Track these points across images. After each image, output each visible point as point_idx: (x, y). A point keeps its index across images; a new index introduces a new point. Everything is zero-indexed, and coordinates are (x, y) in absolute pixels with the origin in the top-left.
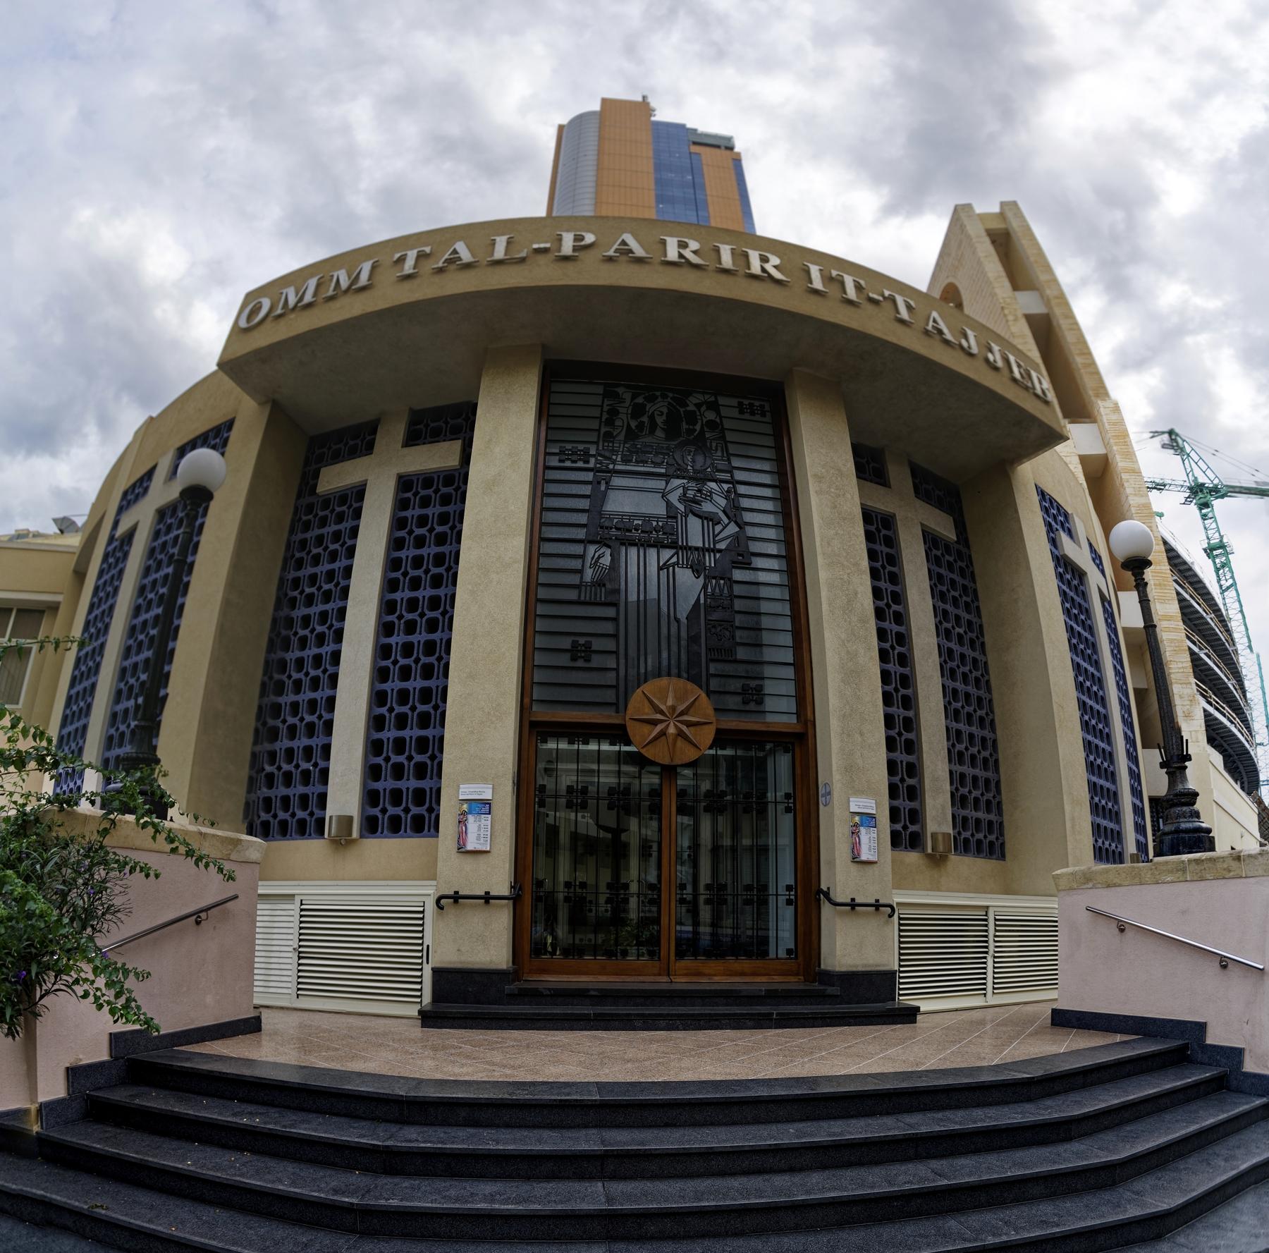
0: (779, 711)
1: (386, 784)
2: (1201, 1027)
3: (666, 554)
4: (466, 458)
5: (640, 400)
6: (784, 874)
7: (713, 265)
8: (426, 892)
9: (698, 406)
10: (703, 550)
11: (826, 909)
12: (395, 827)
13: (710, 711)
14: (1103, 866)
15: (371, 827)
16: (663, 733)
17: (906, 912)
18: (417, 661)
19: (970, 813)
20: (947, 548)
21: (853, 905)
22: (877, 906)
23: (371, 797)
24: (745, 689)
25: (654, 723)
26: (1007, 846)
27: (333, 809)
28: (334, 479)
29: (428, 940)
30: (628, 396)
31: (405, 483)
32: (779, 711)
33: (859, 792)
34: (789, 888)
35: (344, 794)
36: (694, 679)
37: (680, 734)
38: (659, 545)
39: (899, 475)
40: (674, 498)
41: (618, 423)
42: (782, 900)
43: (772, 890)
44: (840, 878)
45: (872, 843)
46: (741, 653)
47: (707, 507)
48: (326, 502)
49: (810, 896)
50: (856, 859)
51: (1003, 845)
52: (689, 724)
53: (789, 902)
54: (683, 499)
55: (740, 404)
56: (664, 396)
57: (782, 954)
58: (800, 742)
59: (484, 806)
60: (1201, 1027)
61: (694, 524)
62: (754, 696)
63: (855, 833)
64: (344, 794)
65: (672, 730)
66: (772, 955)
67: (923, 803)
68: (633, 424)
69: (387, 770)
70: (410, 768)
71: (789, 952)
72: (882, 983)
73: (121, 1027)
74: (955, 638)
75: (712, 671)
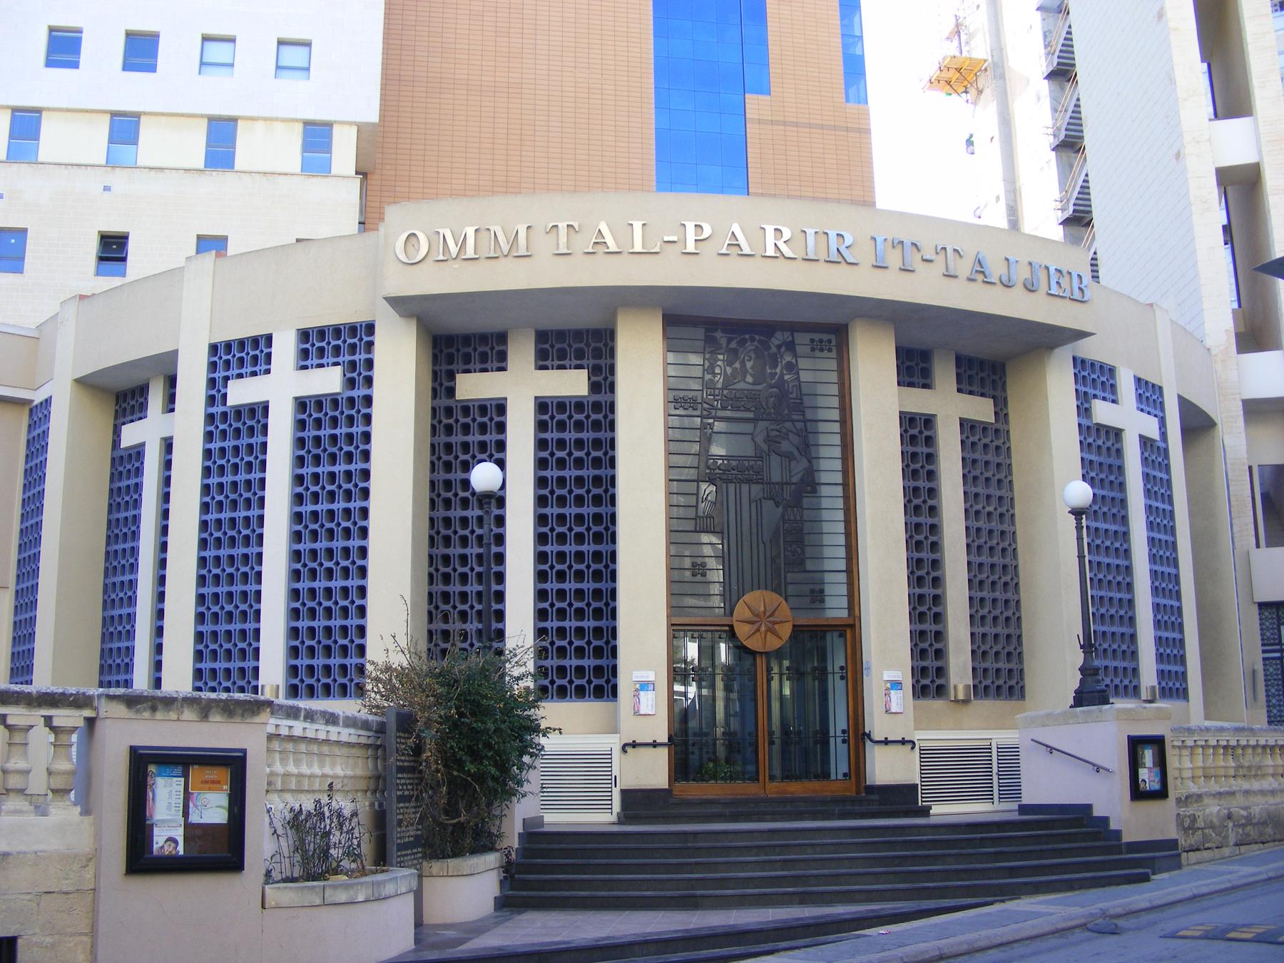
0: (836, 608)
3: (756, 489)
5: (733, 345)
6: (839, 721)
8: (612, 743)
9: (779, 347)
10: (782, 484)
11: (868, 743)
13: (788, 612)
17: (923, 744)
18: (345, 341)
20: (985, 428)
21: (886, 742)
22: (903, 742)
24: (812, 591)
26: (1027, 688)
28: (473, 386)
29: (616, 772)
31: (542, 405)
32: (836, 608)
33: (889, 668)
34: (844, 732)
36: (776, 590)
38: (749, 481)
39: (945, 375)
40: (759, 440)
41: (717, 371)
42: (839, 740)
43: (832, 733)
44: (877, 724)
45: (901, 700)
49: (859, 737)
51: (1022, 687)
52: (772, 615)
53: (844, 741)
54: (768, 440)
55: (812, 341)
57: (840, 777)
58: (850, 629)
59: (644, 686)
61: (775, 460)
62: (818, 596)
63: (637, 696)
65: (763, 628)
66: (833, 777)
67: (947, 662)
68: (729, 370)
71: (845, 775)
72: (908, 791)
74: (1099, 386)
75: (789, 580)
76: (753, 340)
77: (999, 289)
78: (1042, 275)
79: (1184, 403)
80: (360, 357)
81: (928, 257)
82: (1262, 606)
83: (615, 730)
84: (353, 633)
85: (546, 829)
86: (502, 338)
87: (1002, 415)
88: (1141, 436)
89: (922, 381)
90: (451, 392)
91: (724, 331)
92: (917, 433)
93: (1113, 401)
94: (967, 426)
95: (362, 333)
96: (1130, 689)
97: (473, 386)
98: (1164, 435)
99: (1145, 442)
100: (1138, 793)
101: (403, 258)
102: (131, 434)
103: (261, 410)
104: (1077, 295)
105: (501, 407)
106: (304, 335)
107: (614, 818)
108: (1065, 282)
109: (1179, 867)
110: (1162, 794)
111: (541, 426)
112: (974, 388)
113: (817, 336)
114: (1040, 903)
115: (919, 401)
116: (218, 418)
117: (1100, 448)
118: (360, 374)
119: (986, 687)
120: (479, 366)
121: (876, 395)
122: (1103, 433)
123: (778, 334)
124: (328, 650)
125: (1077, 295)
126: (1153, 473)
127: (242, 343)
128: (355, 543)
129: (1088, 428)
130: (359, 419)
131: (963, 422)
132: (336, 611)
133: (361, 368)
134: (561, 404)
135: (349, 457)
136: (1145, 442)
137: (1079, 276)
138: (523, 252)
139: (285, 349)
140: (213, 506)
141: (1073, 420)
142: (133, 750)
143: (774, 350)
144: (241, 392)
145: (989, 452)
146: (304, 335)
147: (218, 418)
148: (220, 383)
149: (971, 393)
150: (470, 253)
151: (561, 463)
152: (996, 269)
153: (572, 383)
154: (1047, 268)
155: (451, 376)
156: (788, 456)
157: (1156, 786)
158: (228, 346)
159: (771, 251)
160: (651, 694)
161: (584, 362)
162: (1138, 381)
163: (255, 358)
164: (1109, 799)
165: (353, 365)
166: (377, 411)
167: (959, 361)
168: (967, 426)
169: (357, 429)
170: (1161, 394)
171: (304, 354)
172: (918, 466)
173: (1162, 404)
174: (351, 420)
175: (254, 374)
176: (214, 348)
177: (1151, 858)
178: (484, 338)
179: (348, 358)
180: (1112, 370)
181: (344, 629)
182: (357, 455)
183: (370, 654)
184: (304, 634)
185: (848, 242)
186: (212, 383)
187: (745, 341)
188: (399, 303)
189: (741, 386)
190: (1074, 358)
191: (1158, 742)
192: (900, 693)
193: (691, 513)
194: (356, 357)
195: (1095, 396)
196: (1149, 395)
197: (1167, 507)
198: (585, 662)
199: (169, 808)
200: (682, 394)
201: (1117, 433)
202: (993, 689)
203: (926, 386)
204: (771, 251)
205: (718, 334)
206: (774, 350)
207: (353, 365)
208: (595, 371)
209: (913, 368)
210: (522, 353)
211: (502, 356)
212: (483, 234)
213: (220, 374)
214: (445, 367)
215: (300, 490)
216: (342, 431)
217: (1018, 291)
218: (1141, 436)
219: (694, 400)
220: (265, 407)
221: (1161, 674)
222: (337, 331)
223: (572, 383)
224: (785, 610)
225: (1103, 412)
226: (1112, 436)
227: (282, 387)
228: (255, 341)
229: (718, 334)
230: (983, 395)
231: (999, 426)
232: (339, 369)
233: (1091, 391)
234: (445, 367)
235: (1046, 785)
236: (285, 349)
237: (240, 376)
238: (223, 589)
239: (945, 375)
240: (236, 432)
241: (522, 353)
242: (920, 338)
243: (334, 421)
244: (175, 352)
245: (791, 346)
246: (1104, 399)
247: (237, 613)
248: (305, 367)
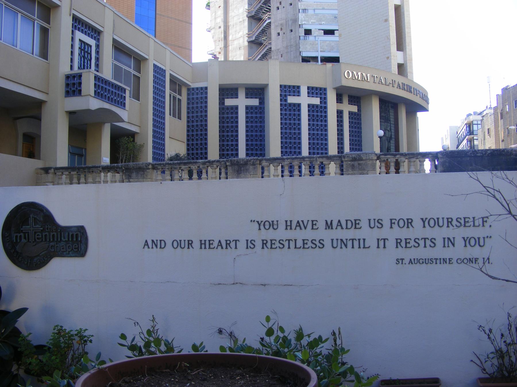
20: (355, 113)
28: (229, 102)
31: (247, 107)
39: (346, 100)
92: (340, 113)
94: (350, 113)
124: (197, 149)
135: (201, 149)
139: (304, 91)
145: (356, 120)
151: (252, 122)
153: (255, 102)
167: (349, 96)
168: (350, 113)
169: (203, 114)
174: (201, 149)
181: (201, 98)
182: (204, 149)
203: (298, 96)
208: (260, 99)
210: (242, 94)
214: (222, 97)
223: (255, 102)
239: (346, 100)
241: (242, 94)
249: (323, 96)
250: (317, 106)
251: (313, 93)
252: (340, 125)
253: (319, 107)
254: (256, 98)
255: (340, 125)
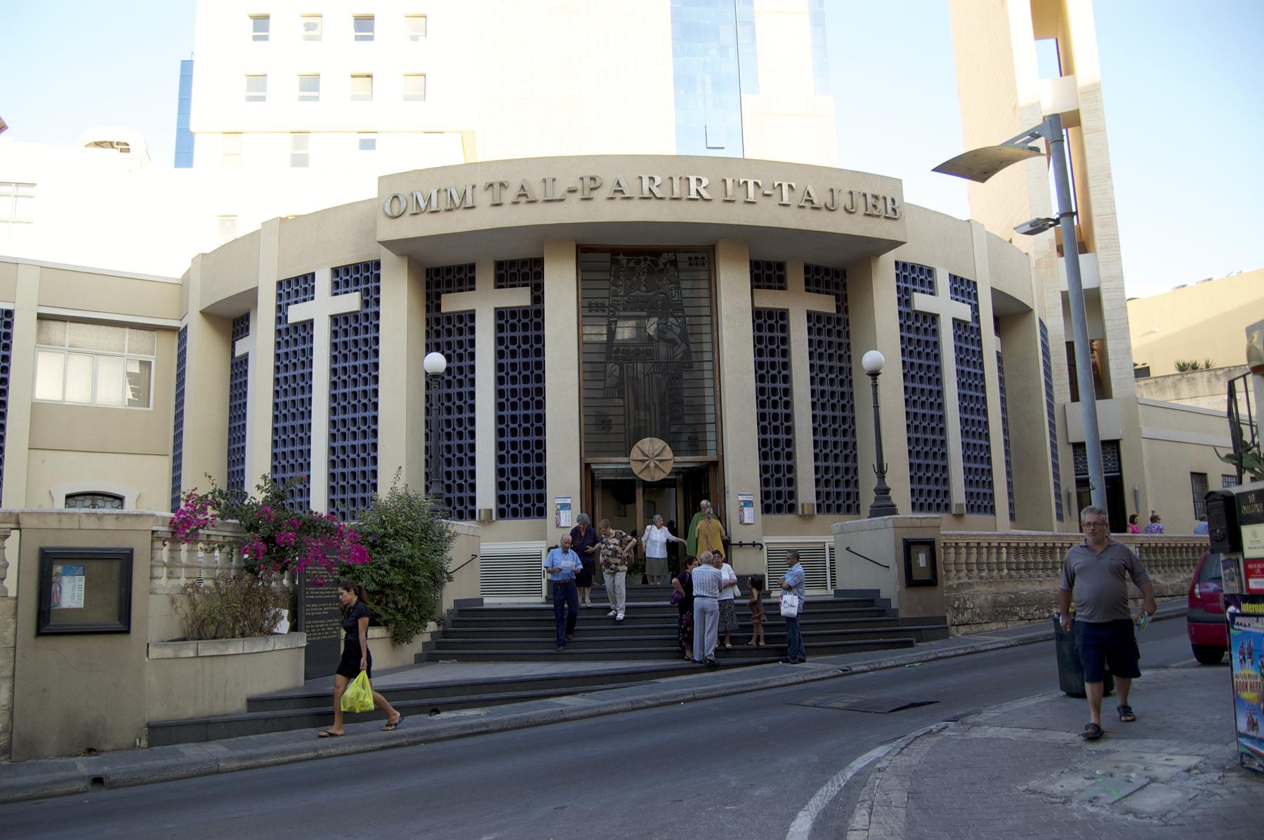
1: (509, 492)
2: (878, 591)
4: (538, 298)
5: (631, 264)
7: (668, 195)
9: (665, 264)
12: (515, 514)
14: (920, 515)
15: (502, 514)
16: (648, 467)
19: (971, 441)
22: (754, 544)
23: (501, 499)
25: (644, 461)
27: (480, 505)
28: (452, 303)
30: (624, 262)
31: (500, 313)
35: (486, 495)
37: (656, 466)
45: (749, 514)
46: (687, 420)
47: (670, 335)
48: (449, 318)
50: (742, 522)
52: (660, 461)
56: (645, 260)
59: (566, 506)
60: (878, 591)
63: (741, 510)
64: (486, 495)
65: (652, 465)
69: (508, 484)
70: (521, 483)
73: (674, 538)
76: (645, 260)
77: (824, 212)
78: (861, 201)
79: (996, 294)
80: (372, 285)
81: (767, 192)
82: (1104, 443)
83: (544, 538)
84: (369, 475)
85: (485, 607)
86: (472, 267)
87: (842, 308)
88: (954, 319)
89: (778, 285)
90: (438, 307)
91: (625, 254)
93: (931, 294)
95: (372, 268)
96: (942, 507)
97: (452, 303)
98: (976, 318)
99: (957, 323)
100: (911, 581)
101: (388, 210)
102: (241, 347)
103: (308, 325)
104: (890, 213)
105: (472, 316)
106: (336, 271)
107: (543, 599)
108: (880, 204)
109: (946, 636)
110: (932, 582)
111: (500, 328)
112: (820, 289)
113: (693, 255)
114: (825, 662)
115: (770, 300)
116: (283, 332)
117: (919, 330)
118: (372, 298)
119: (922, 504)
120: (457, 288)
121: (735, 297)
122: (921, 318)
123: (665, 255)
125: (890, 213)
126: (965, 346)
127: (297, 279)
128: (370, 414)
129: (908, 314)
130: (371, 328)
131: (810, 315)
132: (359, 461)
133: (372, 293)
134: (513, 312)
136: (957, 323)
137: (893, 201)
138: (469, 203)
139: (323, 282)
140: (281, 393)
141: (895, 308)
142: (905, 540)
143: (661, 266)
144: (296, 313)
146: (336, 271)
147: (283, 332)
148: (284, 307)
149: (818, 292)
150: (434, 206)
152: (537, 191)
153: (519, 298)
154: (865, 195)
155: (438, 297)
156: (673, 342)
157: (927, 577)
158: (289, 281)
159: (694, 195)
160: (568, 513)
161: (529, 282)
162: (953, 278)
163: (306, 289)
164: (888, 584)
165: (367, 290)
166: (383, 322)
169: (370, 335)
170: (975, 287)
171: (336, 285)
172: (774, 347)
173: (976, 295)
175: (305, 300)
176: (280, 284)
177: (935, 628)
178: (460, 268)
179: (364, 286)
180: (930, 272)
182: (371, 353)
183: (183, 489)
184: (339, 477)
185: (657, 182)
186: (279, 308)
187: (638, 263)
188: (388, 244)
189: (637, 293)
190: (897, 263)
191: (930, 544)
192: (751, 510)
193: (600, 385)
194: (369, 286)
195: (915, 290)
196: (963, 288)
197: (979, 372)
198: (530, 492)
199: (73, 597)
200: (594, 301)
201: (934, 318)
202: (844, 508)
203: (781, 288)
204: (694, 195)
205: (621, 257)
206: (661, 266)
207: (367, 290)
209: (766, 274)
210: (485, 278)
211: (472, 281)
212: (443, 194)
213: (285, 301)
214: (434, 290)
215: (335, 379)
216: (361, 336)
217: (840, 213)
218: (954, 319)
219: (603, 306)
220: (311, 322)
221: (969, 495)
222: (827, 271)
223: (519, 298)
224: (668, 454)
225: (921, 302)
226: (929, 319)
227: (322, 308)
228: (305, 277)
229: (621, 257)
230: (827, 293)
231: (841, 315)
232: (358, 294)
233: (911, 286)
234: (434, 290)
235: (853, 577)
236: (323, 282)
237: (296, 302)
238: (288, 449)
240: (294, 339)
241: (485, 278)
242: (770, 253)
243: (449, 332)
244: (257, 288)
245: (674, 263)
246: (923, 292)
247: (297, 465)
248: (336, 294)
249: (840, 292)
250: (355, 315)
251: (817, 283)
252: (903, 301)
253: (361, 319)
254: (524, 285)
255: (903, 301)
